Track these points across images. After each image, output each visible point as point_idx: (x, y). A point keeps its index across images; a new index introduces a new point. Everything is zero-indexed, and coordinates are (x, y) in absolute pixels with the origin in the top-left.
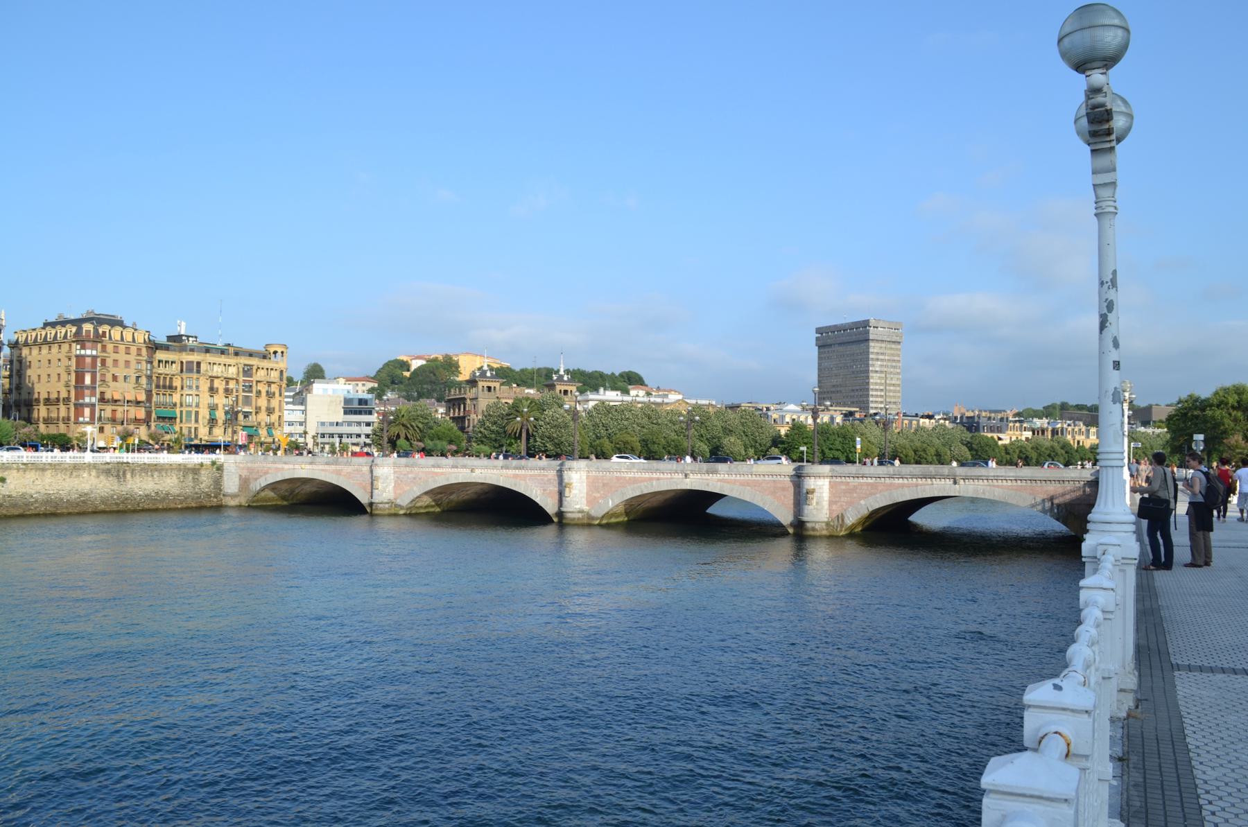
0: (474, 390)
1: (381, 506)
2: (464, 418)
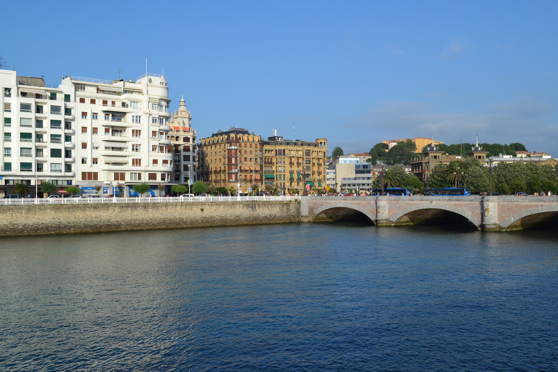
0: (427, 157)
1: (382, 221)
2: (422, 173)
